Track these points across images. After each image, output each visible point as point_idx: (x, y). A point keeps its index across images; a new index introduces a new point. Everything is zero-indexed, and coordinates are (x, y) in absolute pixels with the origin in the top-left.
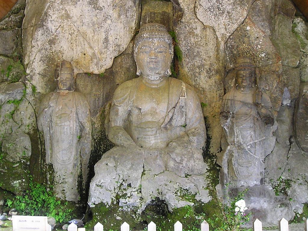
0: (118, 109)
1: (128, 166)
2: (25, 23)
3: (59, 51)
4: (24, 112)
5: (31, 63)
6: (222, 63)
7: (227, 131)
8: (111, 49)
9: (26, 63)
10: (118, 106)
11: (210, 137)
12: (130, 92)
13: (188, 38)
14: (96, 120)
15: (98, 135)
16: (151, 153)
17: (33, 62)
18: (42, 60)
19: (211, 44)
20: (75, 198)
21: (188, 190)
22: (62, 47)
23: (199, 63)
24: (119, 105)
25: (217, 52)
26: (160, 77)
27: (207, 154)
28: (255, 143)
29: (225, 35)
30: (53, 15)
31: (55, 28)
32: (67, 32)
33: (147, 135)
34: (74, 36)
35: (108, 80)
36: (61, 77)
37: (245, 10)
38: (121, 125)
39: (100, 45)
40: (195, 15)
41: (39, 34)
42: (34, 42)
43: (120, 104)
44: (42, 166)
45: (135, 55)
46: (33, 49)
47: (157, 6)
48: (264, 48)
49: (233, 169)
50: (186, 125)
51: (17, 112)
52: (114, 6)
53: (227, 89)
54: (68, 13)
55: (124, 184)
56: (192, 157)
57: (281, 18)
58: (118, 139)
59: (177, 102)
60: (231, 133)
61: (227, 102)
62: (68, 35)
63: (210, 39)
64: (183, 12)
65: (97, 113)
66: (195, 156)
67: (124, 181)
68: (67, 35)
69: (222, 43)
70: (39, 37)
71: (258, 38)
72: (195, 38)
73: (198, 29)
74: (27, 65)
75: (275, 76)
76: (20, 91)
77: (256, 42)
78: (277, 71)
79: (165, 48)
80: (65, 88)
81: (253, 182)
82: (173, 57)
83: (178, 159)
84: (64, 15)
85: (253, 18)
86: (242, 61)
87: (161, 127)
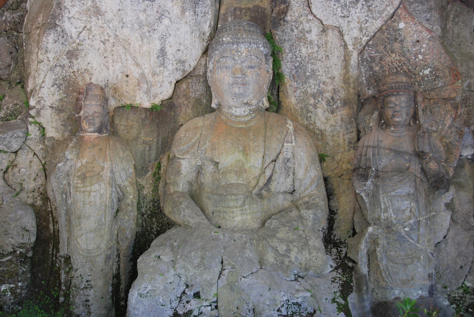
0: (181, 164)
1: (196, 261)
2: (27, 24)
3: (85, 70)
4: (26, 170)
5: (38, 88)
6: (354, 89)
7: (367, 201)
8: (170, 67)
9: (29, 90)
11: (334, 211)
12: (201, 134)
13: (296, 48)
14: (145, 182)
15: (148, 207)
16: (235, 238)
17: (41, 87)
20: (107, 313)
21: (300, 305)
22: (89, 63)
23: (315, 88)
24: (182, 157)
25: (346, 68)
26: (250, 110)
27: (330, 239)
29: (359, 41)
30: (72, 8)
31: (77, 30)
32: (98, 37)
33: (228, 207)
34: (109, 45)
35: (163, 116)
36: (86, 110)
39: (152, 62)
40: (308, 9)
41: (49, 40)
42: (41, 54)
43: (182, 155)
44: (54, 258)
45: (209, 74)
46: (41, 66)
48: (430, 59)
49: (378, 266)
50: (294, 191)
51: (14, 169)
53: (362, 130)
54: (98, 5)
55: (188, 293)
56: (306, 244)
57: (458, 9)
58: (179, 214)
59: (279, 152)
60: (374, 205)
61: (366, 152)
62: (100, 44)
63: (334, 48)
64: (289, 4)
65: (146, 171)
66: (311, 243)
67: (187, 286)
68: (97, 43)
69: (353, 53)
71: (418, 41)
72: (307, 47)
74: (32, 91)
75: (449, 107)
76: (17, 135)
77: (414, 49)
78: (453, 99)
79: (258, 60)
80: (93, 129)
82: (271, 78)
83: (282, 248)
84: (92, 9)
85: (411, 7)
86: (393, 79)
87: (252, 193)
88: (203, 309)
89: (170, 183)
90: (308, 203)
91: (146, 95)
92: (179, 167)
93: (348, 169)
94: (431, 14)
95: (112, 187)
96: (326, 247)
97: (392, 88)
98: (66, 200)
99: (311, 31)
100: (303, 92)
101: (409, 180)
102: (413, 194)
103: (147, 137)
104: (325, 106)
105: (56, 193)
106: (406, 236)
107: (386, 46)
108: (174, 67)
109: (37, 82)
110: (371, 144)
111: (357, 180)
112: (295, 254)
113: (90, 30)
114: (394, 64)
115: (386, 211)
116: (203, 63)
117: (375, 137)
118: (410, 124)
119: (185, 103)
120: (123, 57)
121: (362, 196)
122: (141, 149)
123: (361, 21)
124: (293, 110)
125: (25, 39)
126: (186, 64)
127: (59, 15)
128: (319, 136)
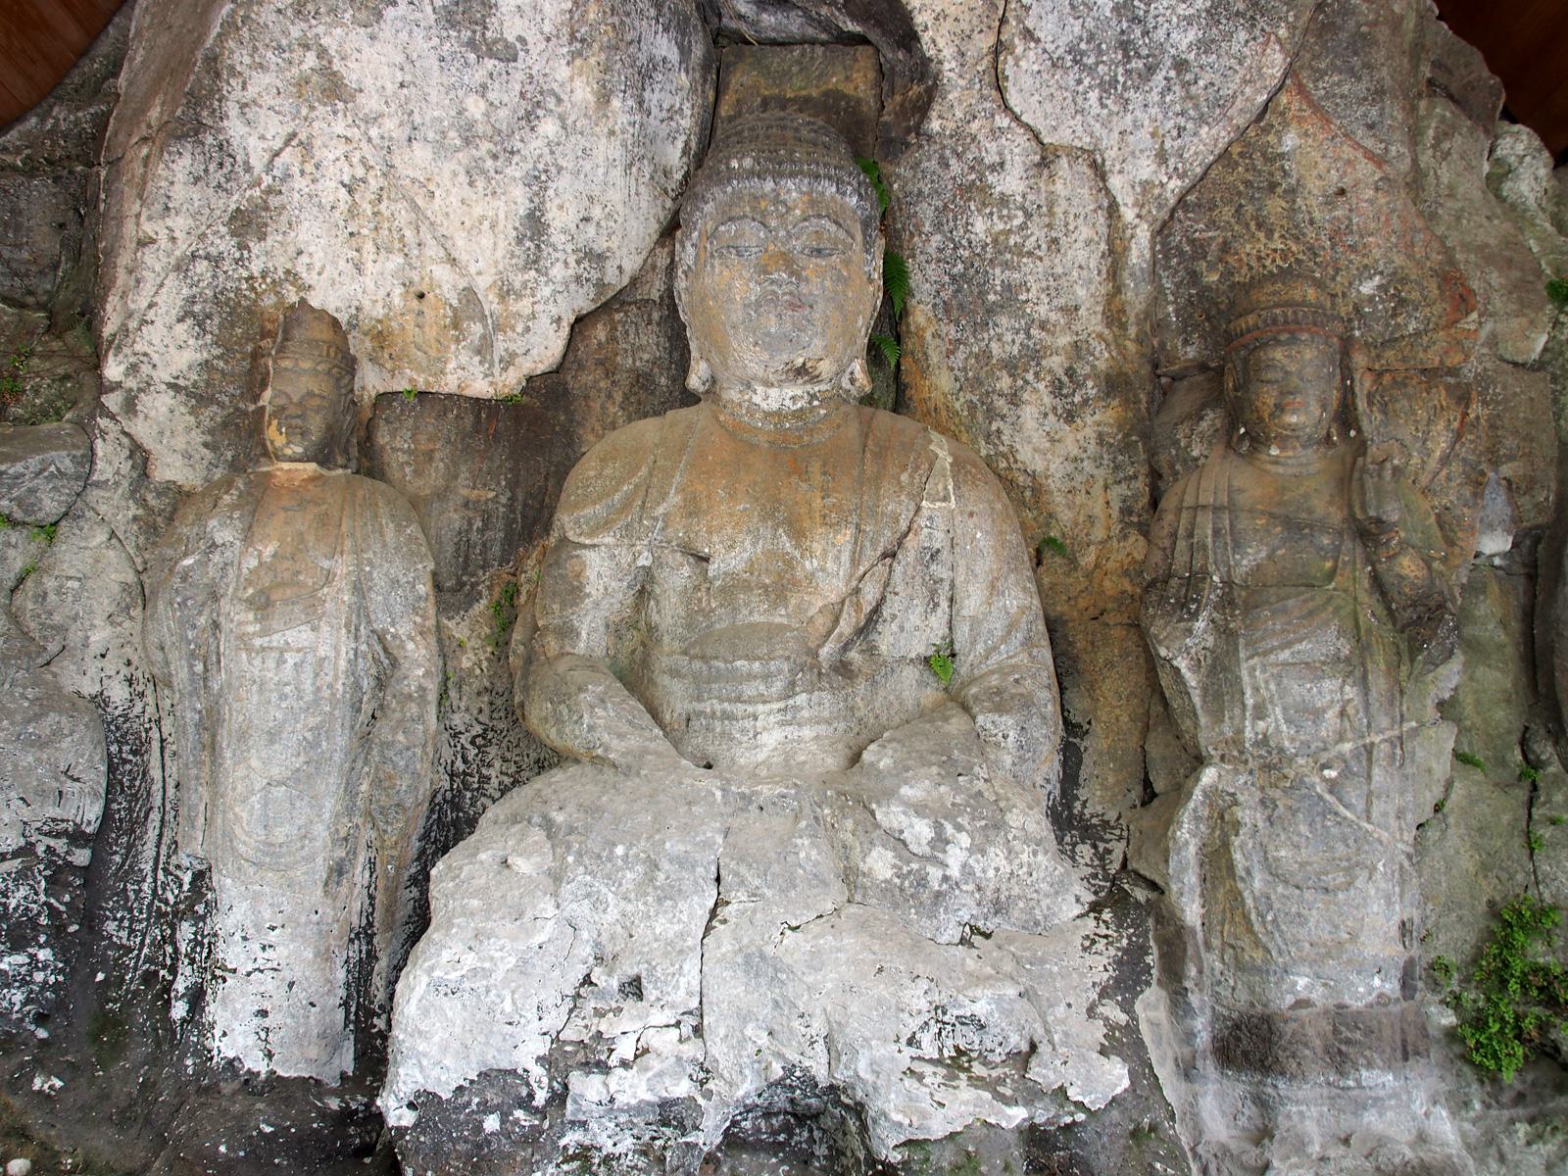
0: (583, 564)
2: (116, 134)
3: (288, 272)
6: (1139, 341)
9: (108, 330)
10: (585, 546)
13: (955, 219)
18: (194, 315)
19: (1080, 244)
22: (300, 253)
28: (1370, 753)
29: (1156, 191)
33: (739, 700)
35: (532, 437)
37: (1279, 40)
38: (599, 652)
46: (148, 256)
47: (795, 69)
49: (1237, 897)
52: (579, 42)
53: (1165, 471)
55: (602, 984)
56: (998, 825)
60: (1218, 696)
66: (1014, 819)
70: (180, 192)
71: (1342, 192)
73: (1007, 166)
75: (1440, 396)
78: (1453, 372)
80: (299, 450)
81: (1370, 987)
84: (315, 78)
85: (1321, 85)
86: (1274, 293)
88: (654, 1039)
89: (546, 627)
90: (999, 692)
91: (477, 358)
92: (578, 576)
93: (1123, 592)
94: (1382, 109)
95: (356, 638)
96: (1060, 841)
97: (1275, 321)
98: (205, 680)
99: (1002, 164)
100: (977, 357)
101: (1337, 610)
102: (1348, 660)
103: (475, 491)
104: (1047, 400)
105: (174, 655)
106: (1327, 797)
107: (1241, 206)
108: (571, 272)
109: (132, 306)
110: (1207, 498)
111: (1162, 617)
112: (962, 856)
113: (307, 147)
114: (1268, 263)
115: (1260, 713)
116: (662, 261)
117: (1217, 479)
118: (1329, 436)
119: (602, 384)
120: (408, 233)
121: (1177, 670)
122: (457, 525)
123: (1161, 132)
124: (944, 413)
125: (106, 181)
126: (608, 264)
127: (211, 93)
128: (1028, 494)
